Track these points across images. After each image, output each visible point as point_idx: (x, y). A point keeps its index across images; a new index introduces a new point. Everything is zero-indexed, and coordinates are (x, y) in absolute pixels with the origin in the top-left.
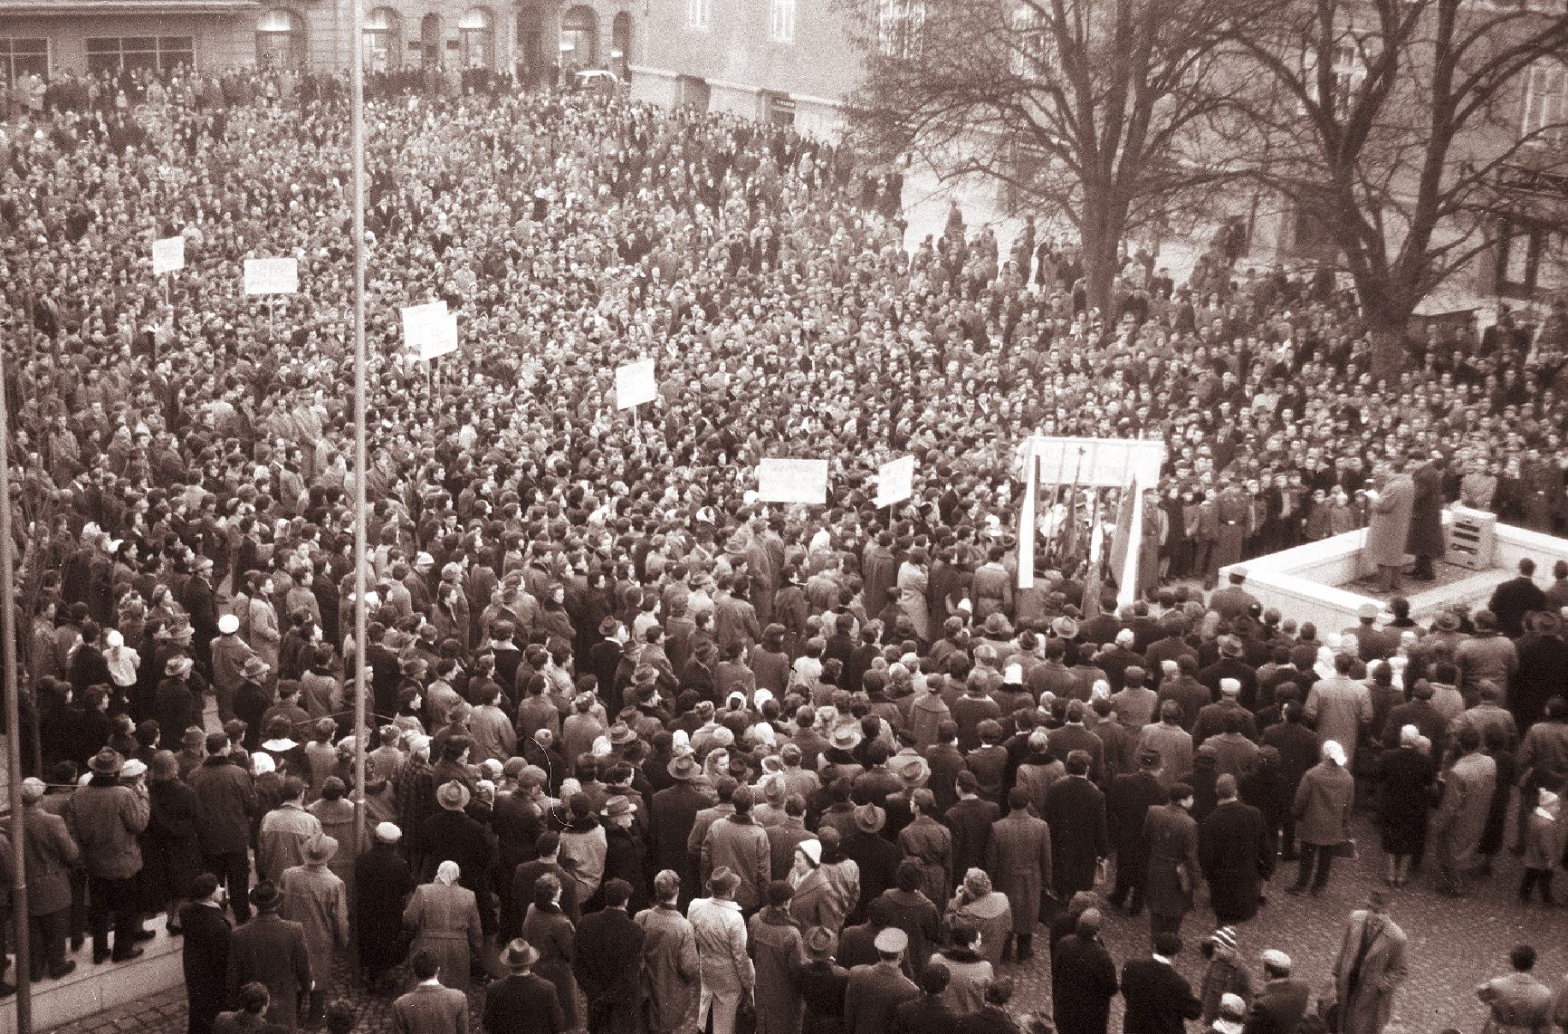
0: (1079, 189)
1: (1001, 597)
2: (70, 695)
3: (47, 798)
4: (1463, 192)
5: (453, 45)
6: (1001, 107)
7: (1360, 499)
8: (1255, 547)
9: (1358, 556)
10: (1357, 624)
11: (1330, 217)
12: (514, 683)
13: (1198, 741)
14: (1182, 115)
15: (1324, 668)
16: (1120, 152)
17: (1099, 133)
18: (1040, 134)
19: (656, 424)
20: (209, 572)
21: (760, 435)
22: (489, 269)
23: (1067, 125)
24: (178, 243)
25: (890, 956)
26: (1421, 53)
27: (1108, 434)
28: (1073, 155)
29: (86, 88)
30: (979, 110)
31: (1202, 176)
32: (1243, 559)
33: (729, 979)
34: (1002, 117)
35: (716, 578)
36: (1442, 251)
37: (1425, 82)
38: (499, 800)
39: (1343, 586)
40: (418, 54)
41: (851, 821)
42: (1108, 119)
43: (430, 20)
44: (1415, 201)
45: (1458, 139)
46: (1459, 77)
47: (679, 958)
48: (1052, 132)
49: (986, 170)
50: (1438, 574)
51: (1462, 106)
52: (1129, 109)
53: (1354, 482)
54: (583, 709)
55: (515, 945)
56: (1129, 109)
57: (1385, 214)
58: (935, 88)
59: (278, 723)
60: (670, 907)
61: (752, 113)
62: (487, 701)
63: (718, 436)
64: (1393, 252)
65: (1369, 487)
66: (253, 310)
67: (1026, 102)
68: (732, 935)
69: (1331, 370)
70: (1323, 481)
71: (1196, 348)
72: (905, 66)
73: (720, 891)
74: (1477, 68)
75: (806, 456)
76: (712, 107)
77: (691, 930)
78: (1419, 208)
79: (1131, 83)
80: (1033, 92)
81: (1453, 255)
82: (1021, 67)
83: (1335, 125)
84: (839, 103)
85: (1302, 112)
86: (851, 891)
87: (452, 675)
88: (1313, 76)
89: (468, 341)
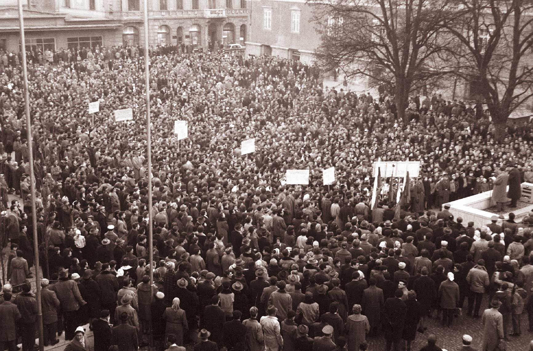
0: (394, 78)
1: (364, 214)
2: (59, 251)
3: (50, 285)
4: (525, 76)
5: (187, 37)
6: (367, 51)
7: (490, 180)
8: (454, 197)
9: (490, 199)
10: (491, 222)
11: (480, 86)
12: (205, 245)
13: (433, 262)
14: (429, 52)
15: (477, 237)
16: (408, 66)
17: (400, 60)
18: (380, 61)
19: (252, 160)
20: (104, 210)
21: (287, 163)
22: (199, 110)
23: (390, 57)
24: (97, 104)
25: (111, 230)
26: (508, 30)
27: (405, 160)
28: (392, 67)
29: (67, 54)
30: (360, 53)
31: (437, 73)
32: (450, 201)
33: (275, 343)
34: (368, 55)
35: (272, 209)
36: (517, 96)
37: (510, 40)
38: (200, 285)
39: (484, 210)
40: (176, 40)
41: (316, 289)
42: (403, 55)
43: (180, 29)
44: (508, 80)
45: (522, 59)
46: (522, 38)
47: (257, 336)
48: (385, 60)
49: (362, 73)
50: (517, 205)
51: (523, 47)
52: (411, 51)
53: (488, 175)
54: (228, 253)
55: (202, 331)
56: (411, 51)
57: (498, 85)
58: (345, 47)
59: (125, 261)
60: (255, 319)
61: (286, 56)
62: (196, 253)
63: (269, 163)
64: (500, 98)
65: (493, 176)
66: (120, 125)
67: (376, 50)
68: (275, 328)
69: (480, 137)
70: (477, 174)
71: (434, 131)
72: (335, 39)
73: (271, 313)
74: (527, 35)
75: (303, 169)
76: (273, 54)
77: (261, 327)
78: (509, 82)
79: (411, 42)
80: (378, 47)
81: (521, 98)
82: (375, 39)
83: (480, 56)
84: (313, 52)
85: (469, 51)
86: (316, 313)
87: (183, 244)
88: (472, 38)
89: (191, 134)
